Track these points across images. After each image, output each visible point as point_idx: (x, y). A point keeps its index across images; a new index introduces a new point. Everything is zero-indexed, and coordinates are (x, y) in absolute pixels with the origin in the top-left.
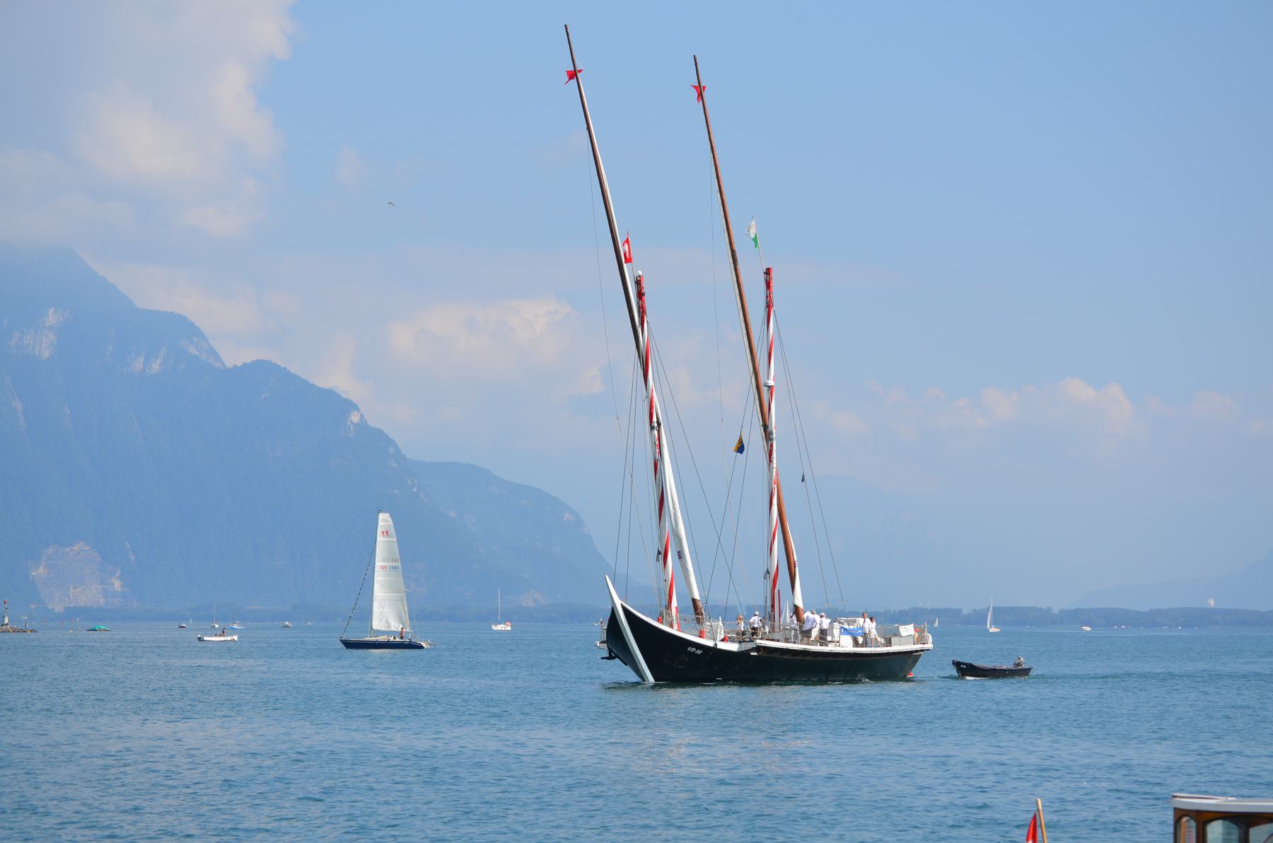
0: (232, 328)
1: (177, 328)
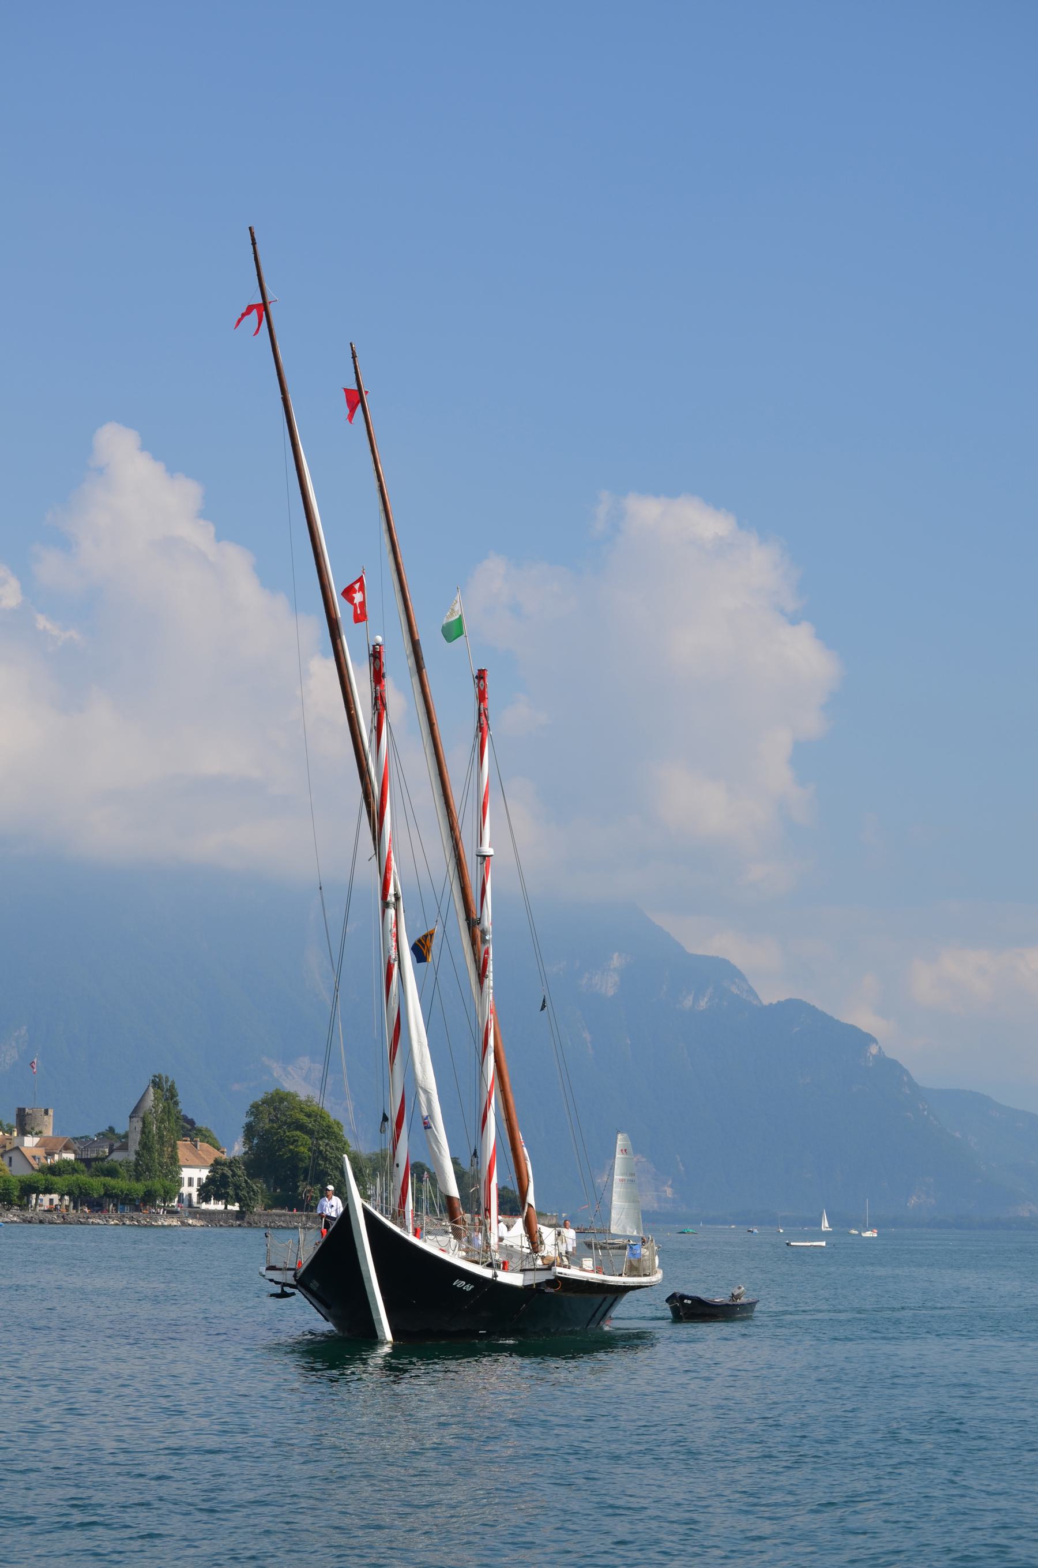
0: (768, 970)
1: (722, 970)
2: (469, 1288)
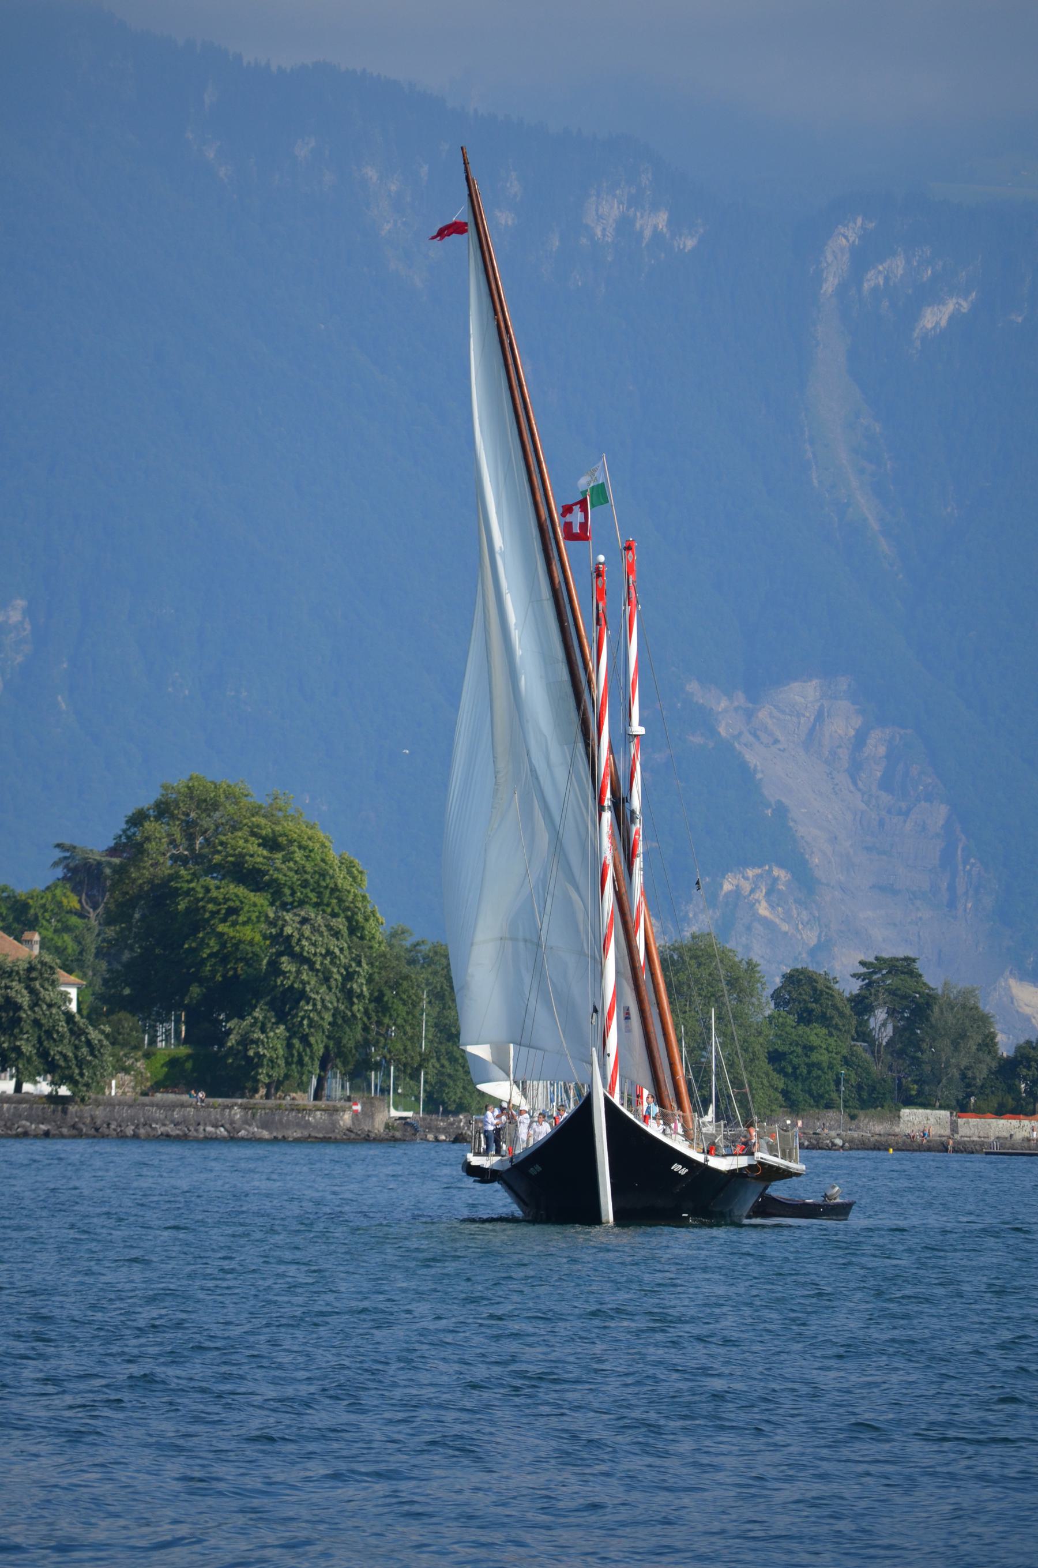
2: (684, 1171)
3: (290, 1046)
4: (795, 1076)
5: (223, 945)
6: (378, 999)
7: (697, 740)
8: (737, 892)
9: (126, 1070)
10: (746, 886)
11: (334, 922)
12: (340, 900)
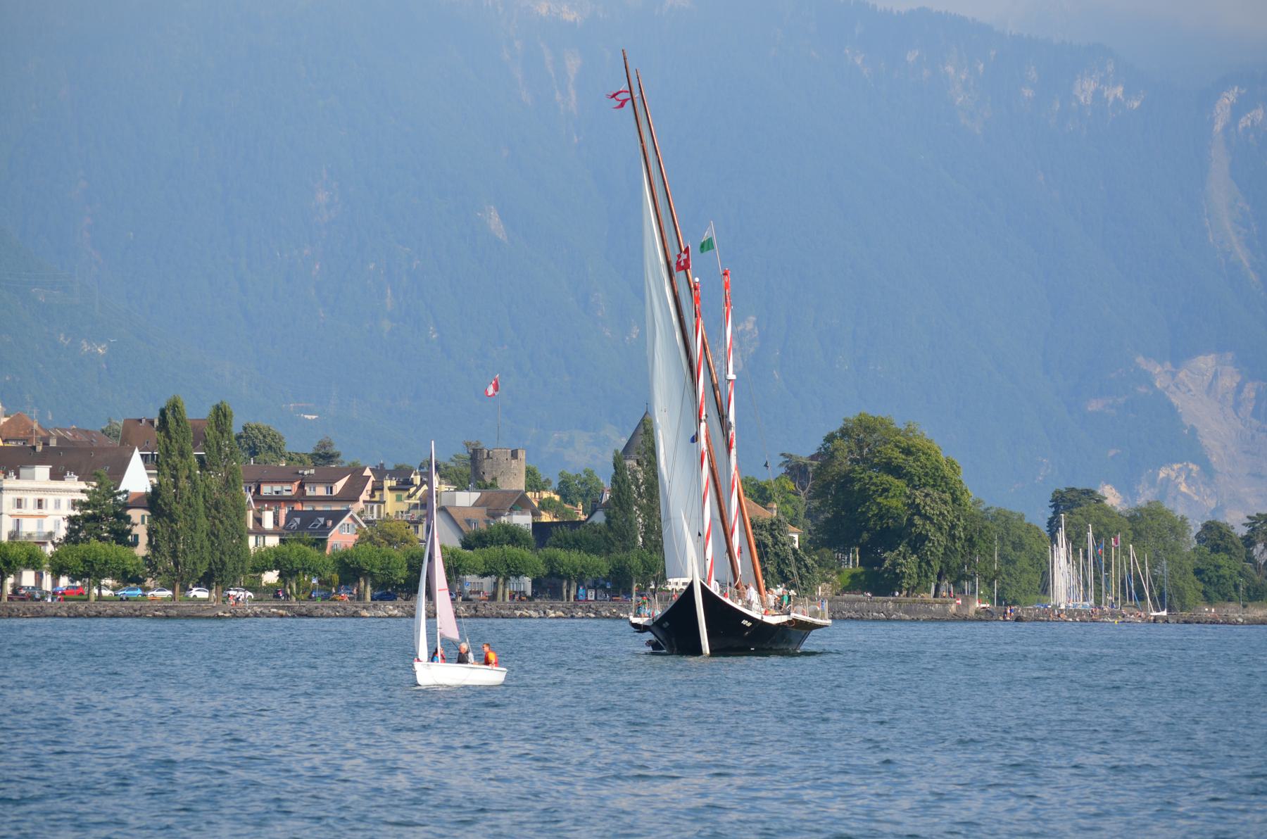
2: (749, 624)
3: (920, 567)
4: (1210, 582)
5: (880, 510)
6: (970, 540)
7: (1142, 390)
8: (1168, 478)
9: (827, 581)
10: (1173, 475)
11: (943, 496)
12: (947, 484)
